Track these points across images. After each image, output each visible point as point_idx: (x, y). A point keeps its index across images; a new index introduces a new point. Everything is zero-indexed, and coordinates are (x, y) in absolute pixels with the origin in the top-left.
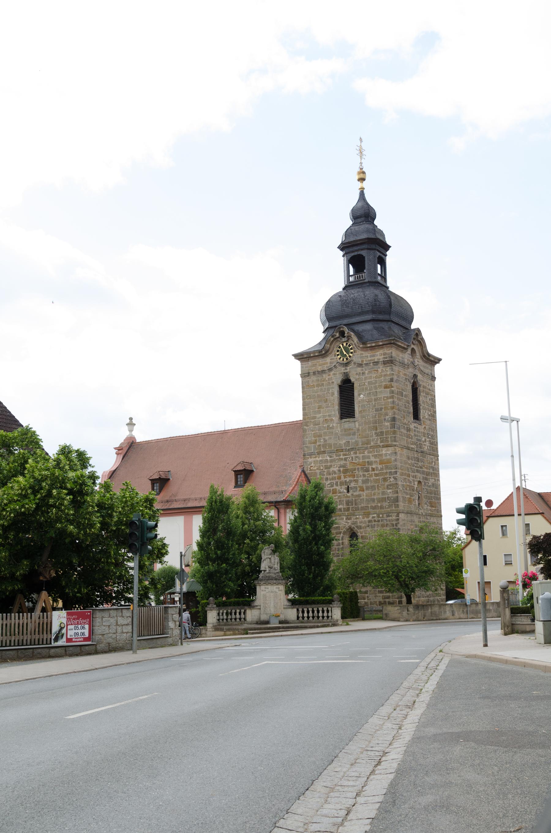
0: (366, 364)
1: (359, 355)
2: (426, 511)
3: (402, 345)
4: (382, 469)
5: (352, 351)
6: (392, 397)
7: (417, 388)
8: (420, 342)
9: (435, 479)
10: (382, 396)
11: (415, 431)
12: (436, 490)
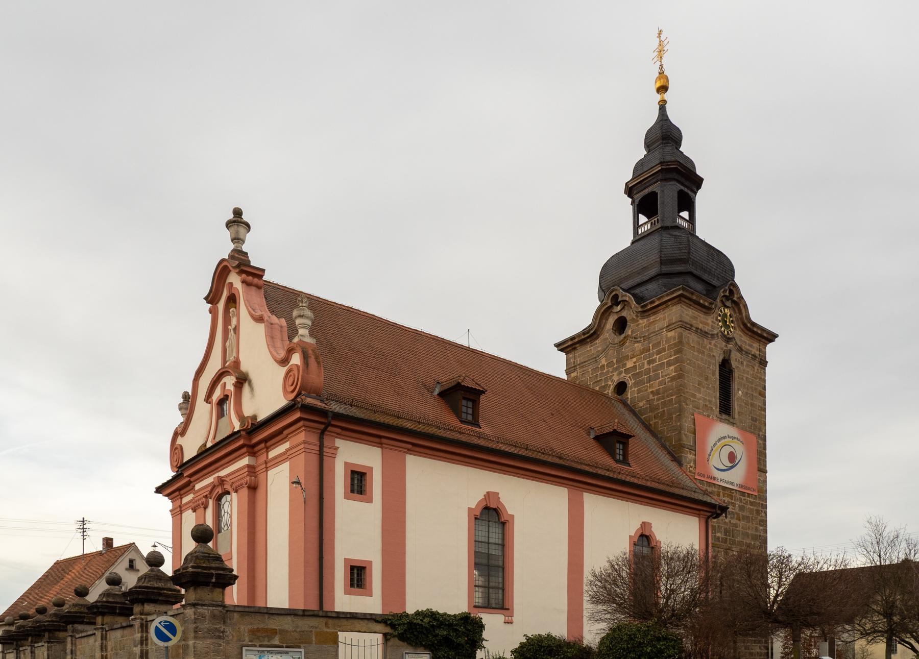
8: (734, 302)
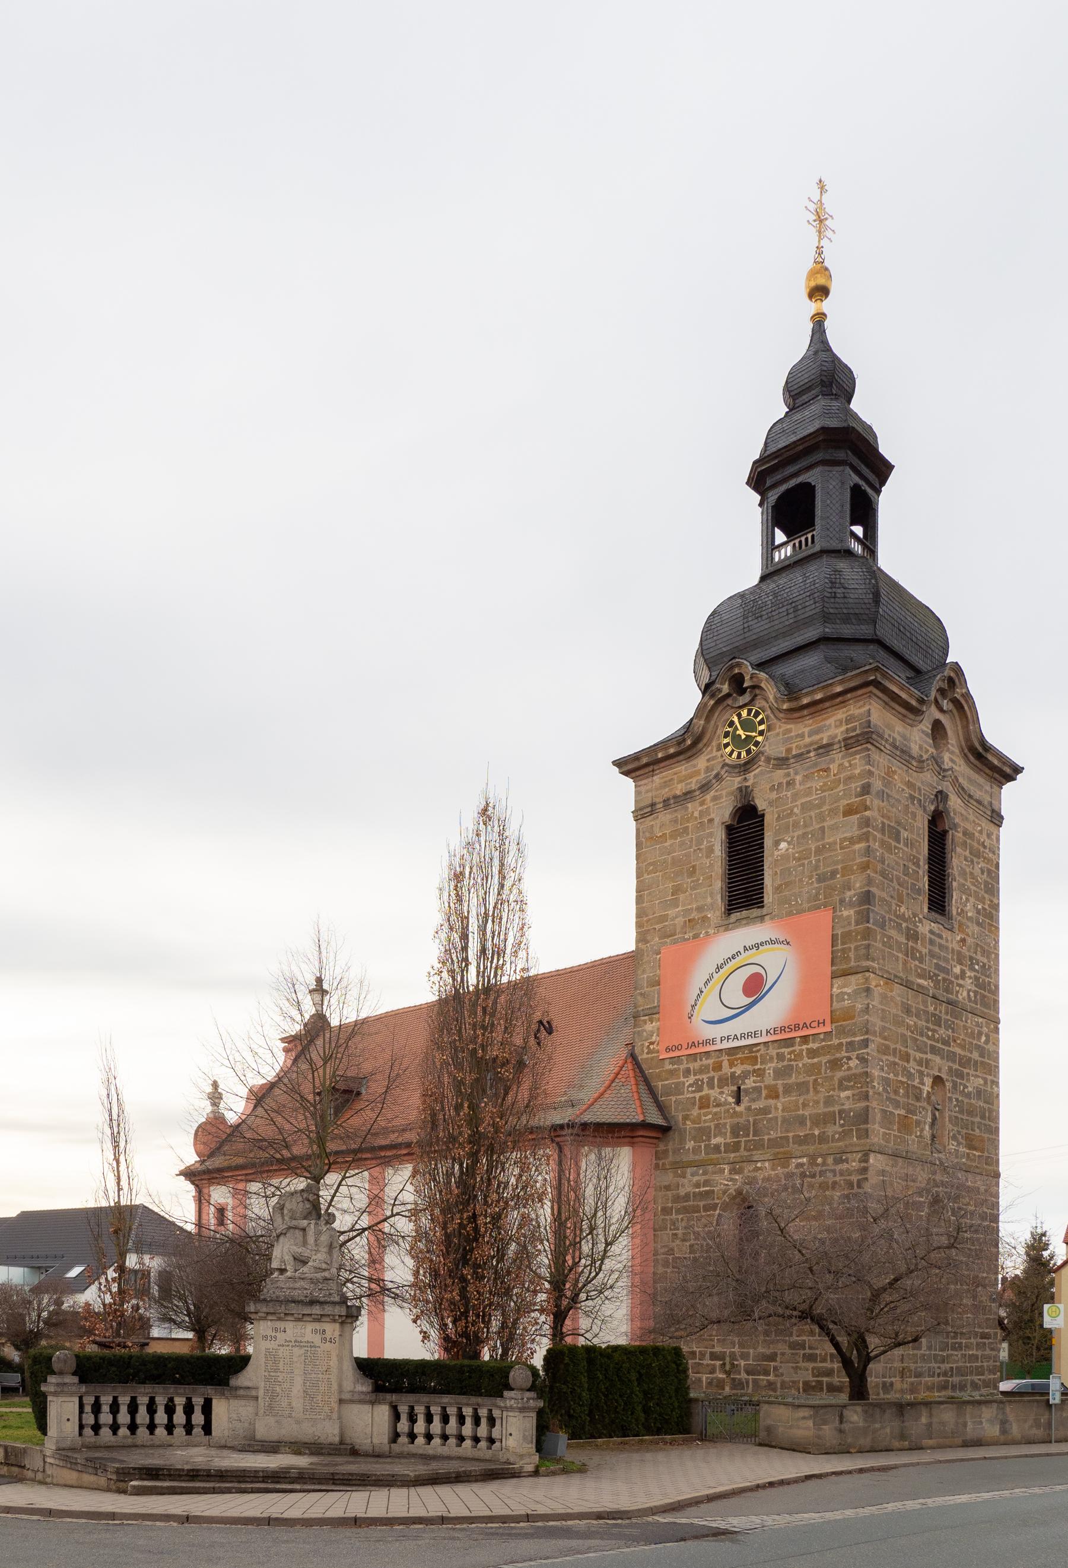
0: (799, 756)
1: (780, 736)
3: (904, 695)
5: (762, 727)
6: (865, 837)
7: (945, 833)
8: (956, 702)
9: (985, 1080)
11: (932, 942)
12: (986, 1106)
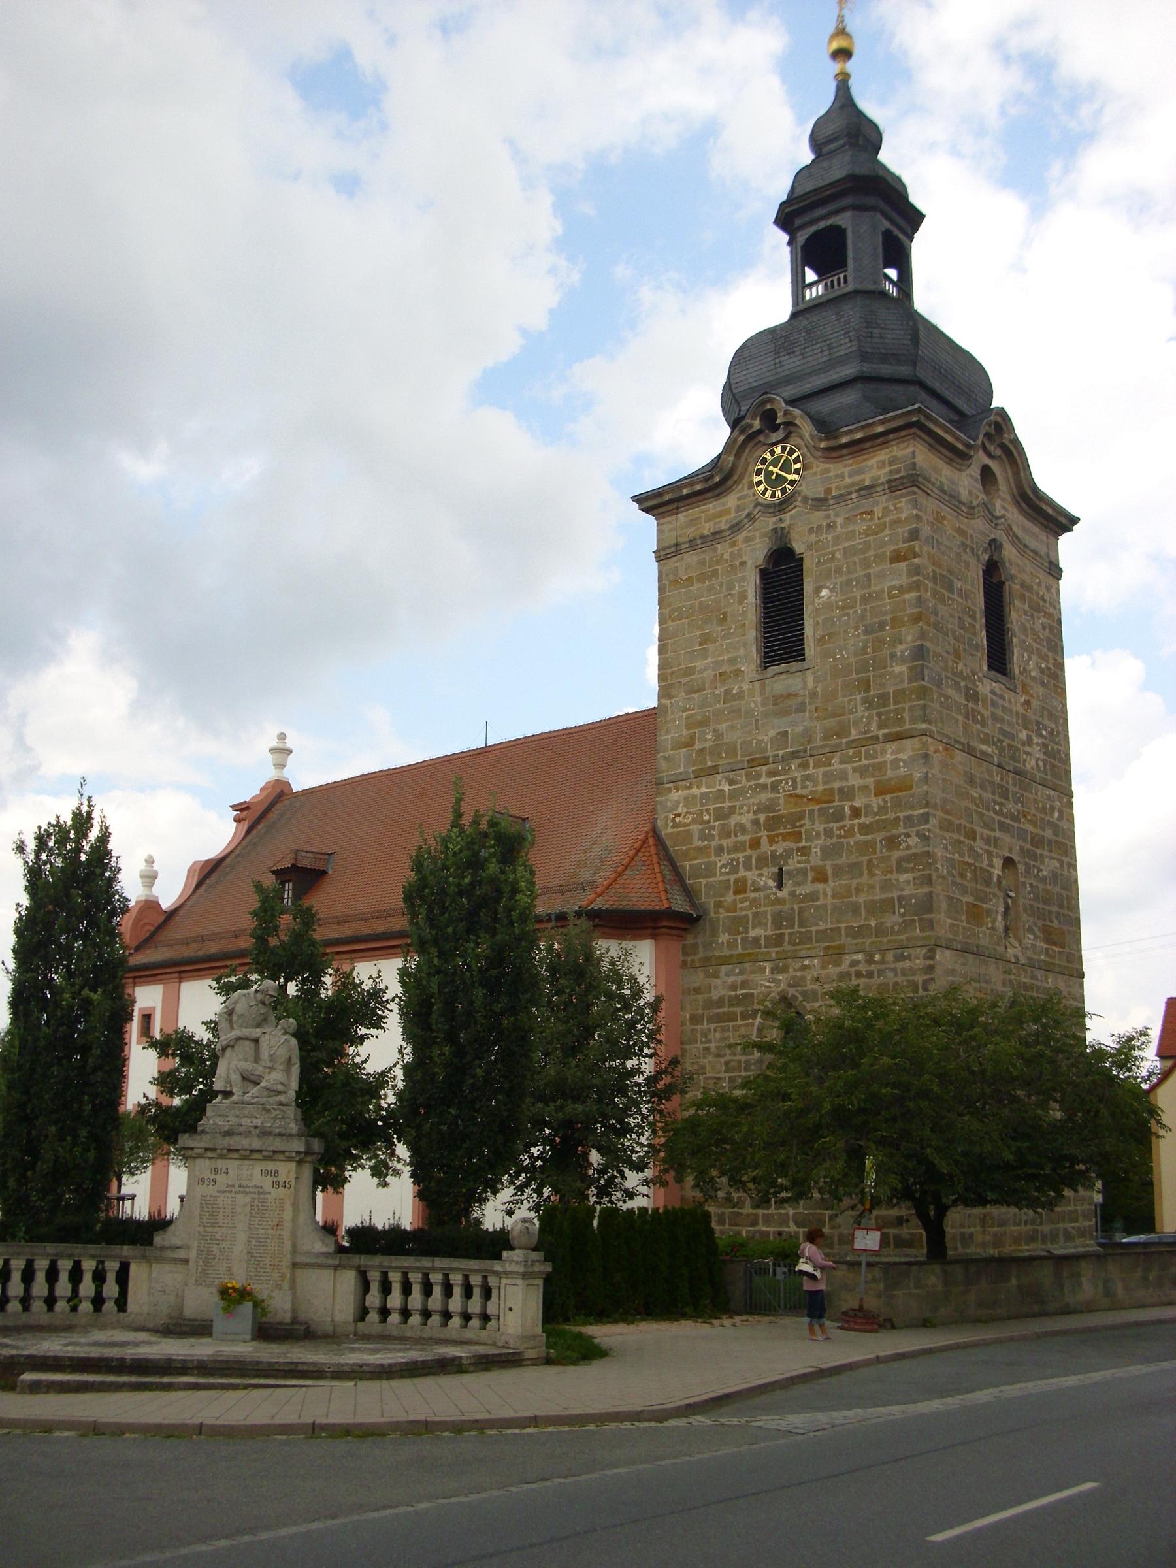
0: (840, 498)
2: (1029, 954)
4: (883, 809)
5: (798, 466)
6: (916, 586)
7: (1001, 584)
10: (887, 584)
12: (1064, 893)
